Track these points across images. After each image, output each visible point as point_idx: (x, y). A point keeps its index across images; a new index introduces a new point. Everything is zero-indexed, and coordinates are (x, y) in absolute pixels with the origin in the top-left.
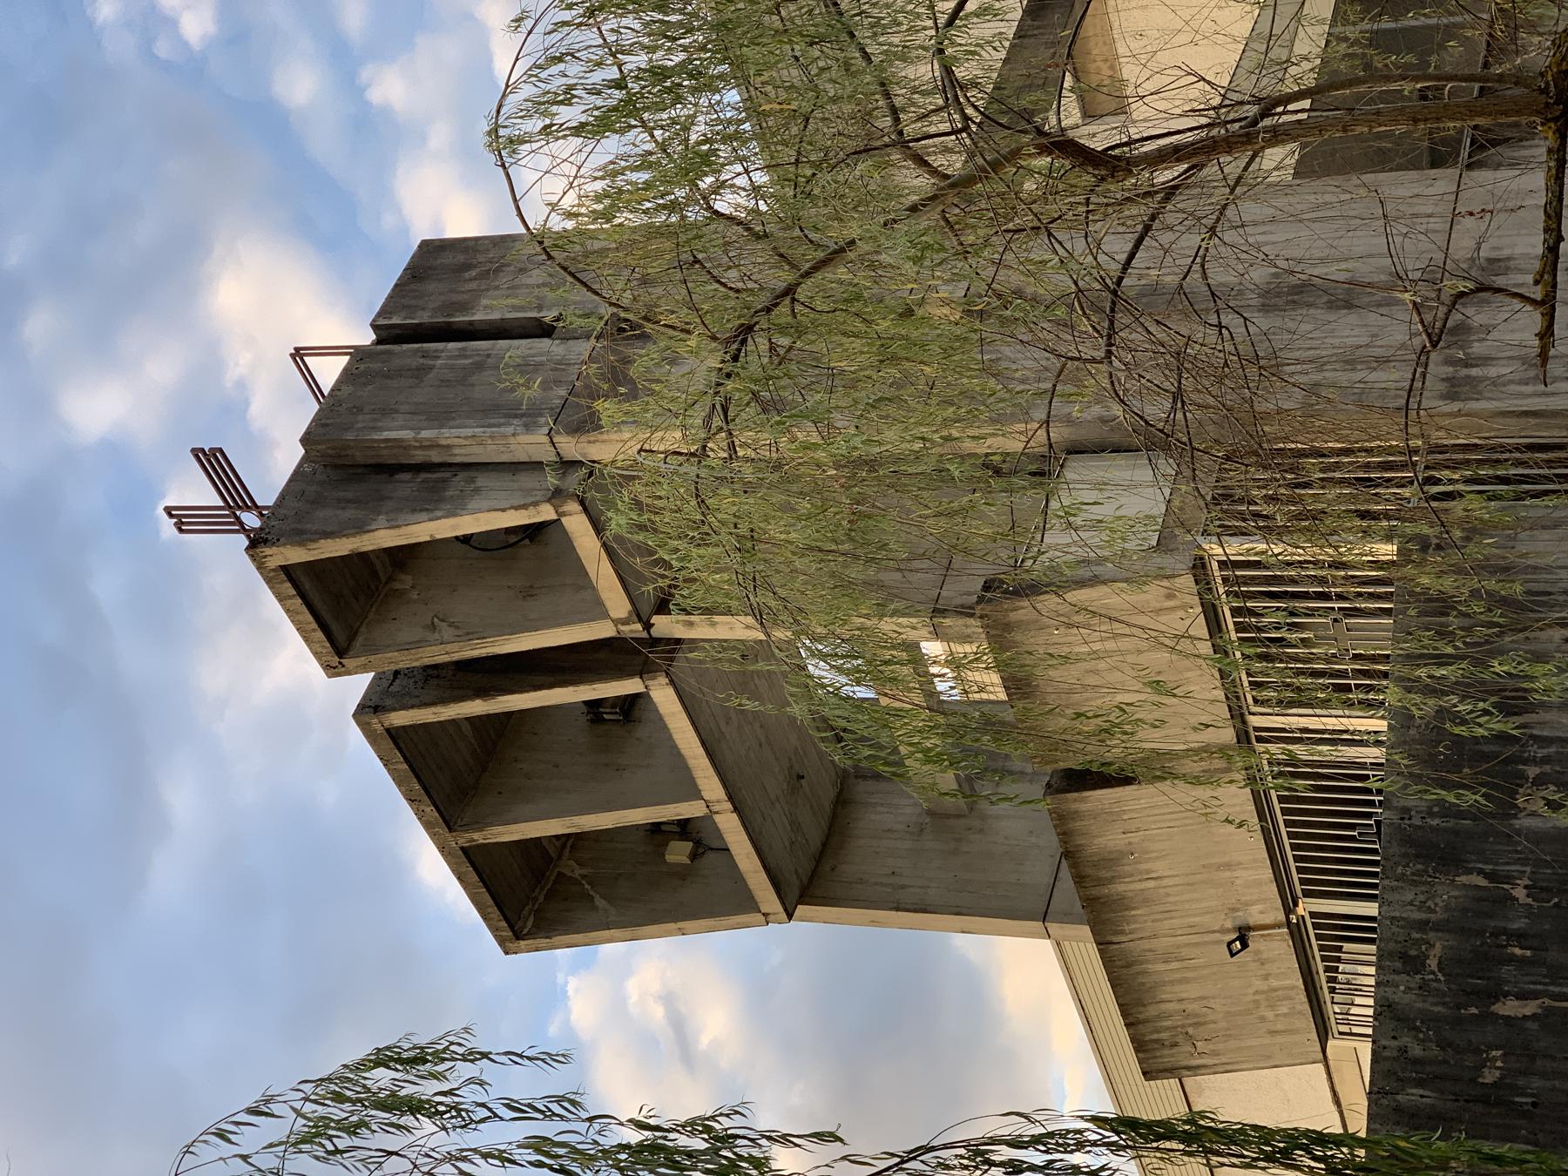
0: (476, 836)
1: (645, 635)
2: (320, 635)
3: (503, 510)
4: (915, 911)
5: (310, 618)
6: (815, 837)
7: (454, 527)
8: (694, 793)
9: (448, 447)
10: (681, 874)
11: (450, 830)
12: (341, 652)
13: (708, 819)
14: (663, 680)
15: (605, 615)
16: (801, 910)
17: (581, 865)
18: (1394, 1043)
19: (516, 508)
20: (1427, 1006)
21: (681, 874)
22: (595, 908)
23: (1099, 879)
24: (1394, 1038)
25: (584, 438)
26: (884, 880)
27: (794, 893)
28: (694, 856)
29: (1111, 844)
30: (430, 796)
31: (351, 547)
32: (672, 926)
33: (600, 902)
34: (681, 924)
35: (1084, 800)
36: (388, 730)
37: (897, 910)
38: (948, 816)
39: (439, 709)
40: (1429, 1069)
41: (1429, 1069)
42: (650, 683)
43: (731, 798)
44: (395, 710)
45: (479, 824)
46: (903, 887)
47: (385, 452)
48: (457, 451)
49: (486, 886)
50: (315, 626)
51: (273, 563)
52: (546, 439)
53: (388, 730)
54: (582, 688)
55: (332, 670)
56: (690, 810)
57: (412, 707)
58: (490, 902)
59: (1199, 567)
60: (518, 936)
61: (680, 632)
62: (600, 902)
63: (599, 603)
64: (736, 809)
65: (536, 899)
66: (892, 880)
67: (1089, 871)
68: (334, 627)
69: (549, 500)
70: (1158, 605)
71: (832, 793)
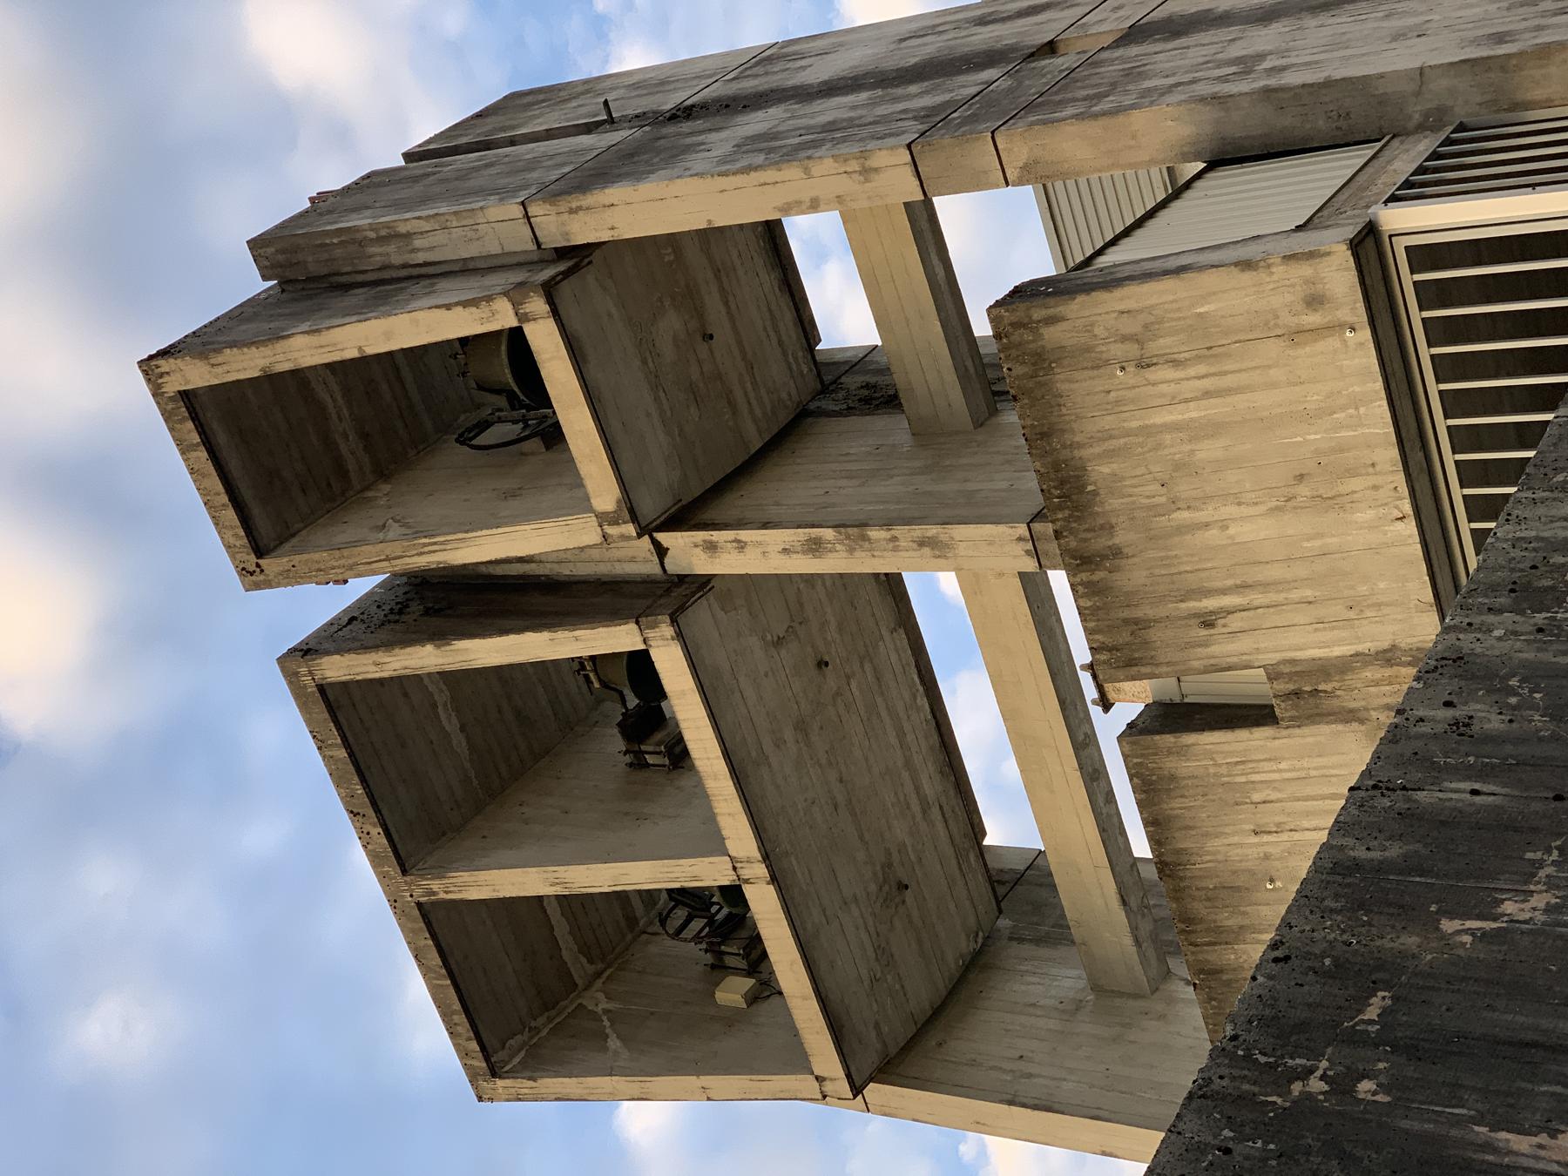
0: (435, 885)
1: (653, 568)
2: (230, 515)
3: (448, 307)
4: (1036, 1107)
5: (220, 487)
6: (921, 995)
7: (388, 335)
8: (714, 844)
9: (408, 236)
10: (730, 1020)
11: (404, 872)
12: (260, 552)
13: (734, 894)
14: (667, 630)
15: (584, 505)
16: (872, 1090)
17: (609, 998)
18: (1449, 713)
19: (465, 304)
20: (1548, 657)
21: (730, 1020)
22: (605, 1049)
23: (1218, 930)
24: (1448, 704)
25: (564, 206)
26: (1007, 1066)
27: (868, 1059)
28: (753, 998)
29: (1235, 854)
30: (378, 811)
31: (262, 363)
32: (692, 1081)
33: (614, 1043)
34: (706, 1080)
35: (1182, 752)
36: (321, 689)
37: (1011, 1103)
38: (1121, 994)
39: (380, 656)
40: (1509, 749)
41: (1509, 749)
42: (650, 634)
43: (766, 858)
44: (328, 653)
45: (440, 870)
46: (1030, 1076)
47: (338, 252)
48: (418, 243)
49: (451, 975)
50: (224, 499)
51: (173, 386)
52: (517, 211)
53: (321, 689)
54: (562, 635)
55: (253, 578)
56: (709, 873)
57: (349, 651)
58: (457, 1006)
59: (1368, 245)
60: (494, 1072)
61: (702, 564)
62: (614, 1043)
63: (579, 483)
64: (774, 879)
65: (538, 1030)
66: (1021, 1065)
67: (1199, 908)
68: (256, 511)
69: (505, 294)
70: (1292, 321)
71: (966, 946)
